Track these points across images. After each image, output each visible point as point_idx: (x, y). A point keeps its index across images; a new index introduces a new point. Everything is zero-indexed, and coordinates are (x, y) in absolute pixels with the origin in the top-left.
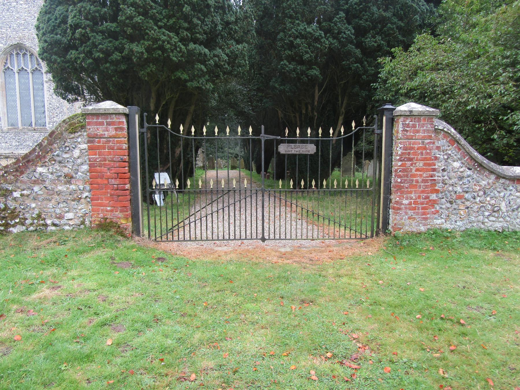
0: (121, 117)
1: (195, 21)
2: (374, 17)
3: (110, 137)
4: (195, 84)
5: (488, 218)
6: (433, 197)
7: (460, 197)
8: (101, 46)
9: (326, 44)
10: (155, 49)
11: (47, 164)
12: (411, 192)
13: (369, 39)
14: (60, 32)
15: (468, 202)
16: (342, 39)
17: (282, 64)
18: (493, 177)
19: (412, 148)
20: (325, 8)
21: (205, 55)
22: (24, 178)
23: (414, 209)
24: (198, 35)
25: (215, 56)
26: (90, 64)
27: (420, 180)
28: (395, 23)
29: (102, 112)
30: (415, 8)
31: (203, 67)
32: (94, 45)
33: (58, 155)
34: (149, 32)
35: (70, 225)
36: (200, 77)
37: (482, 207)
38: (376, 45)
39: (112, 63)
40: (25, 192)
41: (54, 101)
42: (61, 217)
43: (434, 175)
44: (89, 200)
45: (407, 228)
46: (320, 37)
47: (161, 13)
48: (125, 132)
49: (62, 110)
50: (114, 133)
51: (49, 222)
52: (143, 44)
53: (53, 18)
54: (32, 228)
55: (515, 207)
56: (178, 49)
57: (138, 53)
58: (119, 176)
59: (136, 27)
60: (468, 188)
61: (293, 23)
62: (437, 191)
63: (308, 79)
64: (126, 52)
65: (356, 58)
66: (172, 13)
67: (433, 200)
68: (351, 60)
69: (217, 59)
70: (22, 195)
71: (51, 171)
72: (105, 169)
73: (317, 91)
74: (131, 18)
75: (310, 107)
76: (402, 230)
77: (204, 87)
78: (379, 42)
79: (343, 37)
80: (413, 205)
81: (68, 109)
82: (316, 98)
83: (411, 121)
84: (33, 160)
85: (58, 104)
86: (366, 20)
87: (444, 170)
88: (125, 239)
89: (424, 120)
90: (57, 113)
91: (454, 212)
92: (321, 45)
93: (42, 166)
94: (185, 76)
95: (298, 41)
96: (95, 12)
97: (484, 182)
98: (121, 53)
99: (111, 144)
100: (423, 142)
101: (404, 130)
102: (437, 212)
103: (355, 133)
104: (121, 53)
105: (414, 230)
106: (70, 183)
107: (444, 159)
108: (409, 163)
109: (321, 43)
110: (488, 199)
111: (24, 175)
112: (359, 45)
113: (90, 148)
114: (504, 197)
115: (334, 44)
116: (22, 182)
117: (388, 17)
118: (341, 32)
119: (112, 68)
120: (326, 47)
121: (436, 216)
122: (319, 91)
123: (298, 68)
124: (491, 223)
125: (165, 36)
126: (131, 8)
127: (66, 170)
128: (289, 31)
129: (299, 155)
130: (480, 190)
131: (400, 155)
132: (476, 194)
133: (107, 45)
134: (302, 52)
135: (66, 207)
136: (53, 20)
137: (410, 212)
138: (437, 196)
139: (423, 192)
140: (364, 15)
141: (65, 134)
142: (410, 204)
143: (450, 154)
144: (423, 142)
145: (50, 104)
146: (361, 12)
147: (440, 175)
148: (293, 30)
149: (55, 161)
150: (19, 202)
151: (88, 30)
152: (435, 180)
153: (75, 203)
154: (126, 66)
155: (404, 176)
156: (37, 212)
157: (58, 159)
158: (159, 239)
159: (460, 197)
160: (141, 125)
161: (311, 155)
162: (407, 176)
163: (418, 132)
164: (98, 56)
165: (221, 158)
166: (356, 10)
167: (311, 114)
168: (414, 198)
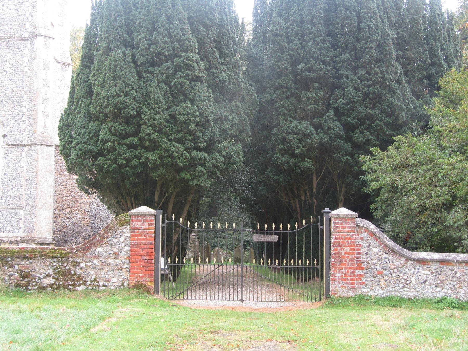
0: (152, 217)
1: (199, 134)
2: (361, 116)
3: (145, 229)
4: (196, 182)
5: (403, 289)
6: (360, 272)
7: (380, 273)
8: (124, 155)
9: (316, 140)
10: (165, 157)
11: (103, 246)
12: (342, 268)
13: (357, 135)
14: (92, 143)
15: (387, 277)
16: (331, 135)
17: (276, 157)
18: (403, 259)
19: (341, 239)
20: (315, 107)
21: (205, 159)
22: (88, 254)
23: (345, 280)
24: (200, 144)
25: (213, 158)
26: (115, 168)
27: (348, 260)
28: (382, 120)
29: (141, 214)
30: (401, 106)
31: (203, 169)
32: (120, 155)
33: (110, 240)
34: (162, 145)
35: (114, 286)
36: (200, 177)
37: (398, 279)
38: (364, 140)
39: (132, 167)
40: (88, 264)
41: (10, 170)
42: (109, 281)
43: (360, 257)
44: (128, 269)
45: (340, 293)
46: (310, 134)
47: (172, 129)
48: (154, 226)
49: (19, 182)
50: (147, 227)
51: (101, 284)
52: (157, 153)
53: (87, 132)
54: (90, 288)
55: (423, 281)
56: (184, 157)
57: (153, 160)
58: (149, 254)
59: (152, 141)
60: (385, 266)
61: (286, 120)
62: (363, 269)
63: (301, 171)
64: (143, 160)
65: (345, 151)
66: (180, 129)
67: (360, 275)
68: (341, 153)
69: (214, 161)
70: (86, 266)
71: (105, 250)
72: (140, 250)
73: (315, 178)
74: (149, 135)
75: (308, 194)
76: (337, 295)
77: (203, 185)
78: (367, 137)
79: (332, 133)
80: (344, 278)
81: (26, 181)
82: (315, 186)
83: (340, 221)
84: (95, 243)
85: (14, 175)
86: (354, 118)
87: (367, 254)
88: (150, 295)
89: (349, 220)
90: (12, 185)
91: (377, 283)
92: (312, 141)
93: (100, 247)
94: (188, 177)
95: (290, 137)
96: (122, 130)
97: (397, 263)
98: (140, 159)
99: (145, 234)
100: (349, 235)
101: (334, 227)
102: (364, 283)
103: (305, 228)
104: (140, 159)
105: (346, 295)
106: (116, 258)
107: (366, 246)
108: (339, 248)
109: (311, 138)
110: (401, 275)
111: (88, 253)
112: (349, 139)
113: (132, 236)
114: (413, 273)
115: (324, 139)
116: (87, 257)
117: (376, 114)
118: (331, 129)
119: (131, 171)
120: (316, 143)
121: (363, 286)
122: (317, 178)
123: (291, 161)
124: (405, 293)
125: (174, 147)
126: (150, 128)
127: (115, 250)
128: (283, 127)
129: (267, 242)
130: (394, 268)
131: (333, 243)
132: (392, 271)
133: (129, 154)
134: (294, 147)
135: (112, 274)
136: (87, 134)
137: (342, 283)
138: (363, 272)
139: (350, 268)
140: (351, 114)
141: (116, 227)
142: (342, 276)
143: (370, 243)
144: (349, 235)
145: (5, 174)
146: (349, 112)
147: (364, 257)
148: (285, 126)
149: (108, 244)
150: (84, 270)
151: (116, 144)
152: (360, 260)
153: (119, 271)
154: (142, 169)
155: (337, 257)
156: (94, 277)
157: (110, 242)
158: (170, 298)
159: (380, 273)
160: (163, 222)
161: (275, 242)
162: (339, 257)
163: (345, 227)
164: (122, 163)
165: (222, 247)
166: (344, 109)
167: (310, 201)
168: (344, 272)
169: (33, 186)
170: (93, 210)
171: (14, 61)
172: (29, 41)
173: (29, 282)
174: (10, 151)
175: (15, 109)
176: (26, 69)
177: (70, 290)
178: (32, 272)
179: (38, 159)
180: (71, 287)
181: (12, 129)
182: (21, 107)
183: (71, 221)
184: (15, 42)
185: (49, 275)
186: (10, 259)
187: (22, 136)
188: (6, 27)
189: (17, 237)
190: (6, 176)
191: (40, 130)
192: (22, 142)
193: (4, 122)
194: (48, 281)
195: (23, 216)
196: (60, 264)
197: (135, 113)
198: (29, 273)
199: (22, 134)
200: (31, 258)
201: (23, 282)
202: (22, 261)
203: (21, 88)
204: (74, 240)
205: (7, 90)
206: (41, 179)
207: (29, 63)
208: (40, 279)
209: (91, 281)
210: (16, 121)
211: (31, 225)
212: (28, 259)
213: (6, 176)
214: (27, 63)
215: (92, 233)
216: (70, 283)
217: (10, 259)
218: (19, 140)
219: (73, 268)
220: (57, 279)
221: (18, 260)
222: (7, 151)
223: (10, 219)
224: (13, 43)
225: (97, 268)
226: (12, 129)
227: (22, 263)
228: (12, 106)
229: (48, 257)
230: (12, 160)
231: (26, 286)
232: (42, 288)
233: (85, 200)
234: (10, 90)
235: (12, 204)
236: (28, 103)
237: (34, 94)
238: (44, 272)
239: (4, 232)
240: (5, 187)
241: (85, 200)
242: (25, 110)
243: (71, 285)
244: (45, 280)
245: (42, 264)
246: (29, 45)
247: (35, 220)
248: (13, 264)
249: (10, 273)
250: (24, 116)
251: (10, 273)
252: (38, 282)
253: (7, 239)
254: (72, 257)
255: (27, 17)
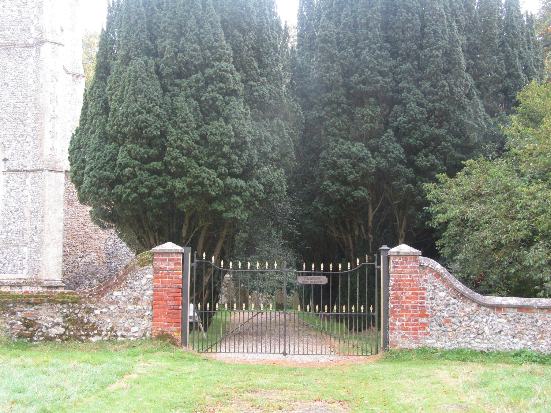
0: (179, 255)
1: (234, 157)
2: (425, 136)
3: (171, 270)
4: (230, 215)
5: (474, 340)
6: (424, 320)
7: (447, 321)
8: (146, 183)
9: (373, 164)
10: (194, 185)
11: (121, 289)
12: (402, 316)
13: (421, 159)
14: (108, 169)
15: (455, 326)
16: (390, 159)
17: (325, 185)
18: (475, 305)
19: (402, 281)
20: (371, 126)
21: (242, 187)
22: (104, 299)
23: (406, 329)
24: (235, 170)
25: (251, 186)
26: (136, 198)
27: (409, 306)
28: (449, 141)
29: (166, 251)
30: (472, 124)
31: (239, 199)
32: (141, 182)
33: (130, 283)
34: (191, 170)
35: (134, 336)
36: (236, 208)
37: (468, 329)
38: (428, 164)
39: (155, 197)
40: (104, 310)
41: (11, 200)
42: (128, 330)
43: (424, 303)
44: (150, 317)
45: (401, 345)
46: (366, 157)
47: (202, 152)
48: (181, 266)
49: (22, 214)
50: (173, 267)
51: (119, 334)
52: (185, 180)
53: (103, 155)
54: (106, 338)
55: (498, 331)
56: (217, 185)
57: (180, 189)
58: (175, 299)
59: (180, 166)
60: (454, 313)
61: (336, 141)
62: (427, 316)
63: (355, 201)
64: (168, 188)
65: (407, 178)
66: (212, 152)
67: (424, 323)
68: (402, 180)
69: (252, 190)
70: (101, 312)
71: (124, 294)
72: (165, 294)
73: (370, 210)
74: (176, 159)
75: (363, 228)
76: (397, 347)
77: (239, 218)
78: (432, 161)
79: (390, 157)
80: (405, 327)
81: (31, 213)
82: (371, 218)
83: (400, 260)
84: (111, 286)
85: (17, 205)
86: (417, 139)
87: (432, 299)
88: (177, 348)
89: (410, 258)
90: (14, 218)
91: (443, 333)
92: (367, 166)
93: (118, 291)
94: (221, 208)
95: (341, 161)
96: (144, 153)
97: (467, 309)
98: (164, 188)
99: (171, 275)
100: (410, 276)
101: (394, 267)
102: (428, 333)
103: (359, 268)
104: (164, 188)
105: (407, 347)
106: (137, 303)
107: (431, 289)
108: (400, 292)
109: (366, 163)
110: (473, 323)
111: (104, 298)
112: (411, 164)
113: (155, 278)
114: (487, 322)
115: (381, 163)
116: (102, 302)
117: (442, 135)
118: (390, 152)
119: (154, 201)
120: (372, 168)
121: (428, 336)
122: (373, 210)
123: (343, 189)
124: (477, 344)
125: (205, 173)
126: (176, 150)
127: (135, 294)
128: (333, 149)
129: (314, 285)
130: (464, 316)
131: (392, 286)
132: (461, 319)
133: (152, 181)
134: (346, 173)
135: (132, 322)
136: (103, 157)
137: (403, 333)
138: (427, 320)
139: (412, 316)
140: (414, 134)
141: (137, 267)
142: (402, 325)
143: (436, 286)
144: (410, 276)
145: (6, 205)
146: (410, 131)
147: (429, 302)
148: (336, 149)
149: (127, 287)
150: (98, 318)
151: (136, 169)
152: (424, 306)
153: (140, 319)
154: (167, 199)
155: (396, 302)
156: (110, 325)
157: (130, 285)
158: (201, 351)
159: (447, 321)
160: (192, 261)
161: (323, 285)
162: (399, 302)
163: (406, 268)
164: (144, 192)
165: (261, 290)
166: (405, 129)
167: (365, 236)
168: (405, 320)
169: (39, 219)
170: (110, 247)
171: (17, 72)
172: (35, 49)
173: (34, 332)
174: (11, 178)
175: (17, 129)
176: (30, 81)
177: (82, 341)
178: (37, 320)
179: (45, 187)
180: (84, 338)
181: (14, 152)
182: (24, 126)
183: (84, 260)
184: (17, 50)
185: (58, 324)
186: (11, 305)
187: (26, 160)
188: (7, 32)
189: (20, 279)
190: (7, 208)
191: (47, 153)
192: (26, 167)
193: (5, 143)
194: (56, 331)
195: (27, 254)
196: (71, 311)
197: (159, 133)
198: (34, 321)
199: (26, 157)
200: (37, 304)
201: (27, 332)
202: (26, 307)
203: (25, 103)
204: (87, 282)
205: (8, 105)
206: (48, 210)
207: (34, 74)
208: (47, 328)
209: (107, 331)
210: (19, 142)
211: (36, 264)
212: (33, 305)
213: (7, 208)
214: (31, 74)
215: (108, 274)
216: (83, 333)
217: (11, 305)
218: (22, 164)
219: (86, 316)
220: (67, 328)
221: (22, 306)
222: (9, 177)
223: (11, 258)
224: (16, 51)
225: (115, 315)
226: (14, 152)
227: (26, 309)
228: (14, 125)
229: (57, 302)
230: (14, 188)
231: (31, 337)
232: (49, 339)
233: (101, 236)
234: (12, 106)
235: (14, 240)
236: (33, 121)
237: (40, 111)
238: (52, 320)
239: (4, 273)
240: (6, 219)
241: (101, 236)
242: (29, 130)
243: (83, 335)
244: (53, 329)
245: (49, 310)
246: (34, 53)
247: (41, 259)
248: (16, 310)
249: (12, 321)
250: (28, 136)
251: (12, 321)
252: (45, 331)
253: (9, 281)
254: (85, 303)
255: (32, 21)
